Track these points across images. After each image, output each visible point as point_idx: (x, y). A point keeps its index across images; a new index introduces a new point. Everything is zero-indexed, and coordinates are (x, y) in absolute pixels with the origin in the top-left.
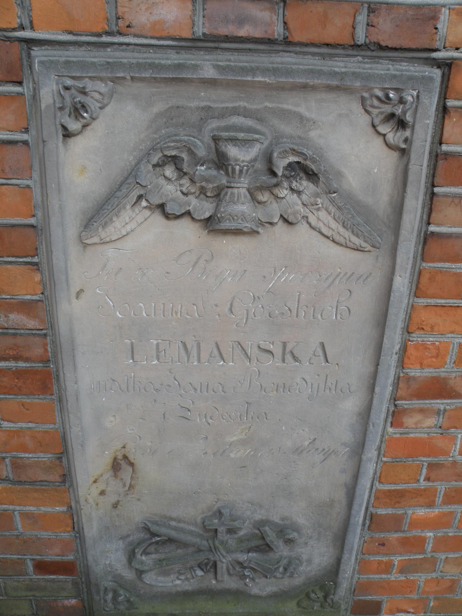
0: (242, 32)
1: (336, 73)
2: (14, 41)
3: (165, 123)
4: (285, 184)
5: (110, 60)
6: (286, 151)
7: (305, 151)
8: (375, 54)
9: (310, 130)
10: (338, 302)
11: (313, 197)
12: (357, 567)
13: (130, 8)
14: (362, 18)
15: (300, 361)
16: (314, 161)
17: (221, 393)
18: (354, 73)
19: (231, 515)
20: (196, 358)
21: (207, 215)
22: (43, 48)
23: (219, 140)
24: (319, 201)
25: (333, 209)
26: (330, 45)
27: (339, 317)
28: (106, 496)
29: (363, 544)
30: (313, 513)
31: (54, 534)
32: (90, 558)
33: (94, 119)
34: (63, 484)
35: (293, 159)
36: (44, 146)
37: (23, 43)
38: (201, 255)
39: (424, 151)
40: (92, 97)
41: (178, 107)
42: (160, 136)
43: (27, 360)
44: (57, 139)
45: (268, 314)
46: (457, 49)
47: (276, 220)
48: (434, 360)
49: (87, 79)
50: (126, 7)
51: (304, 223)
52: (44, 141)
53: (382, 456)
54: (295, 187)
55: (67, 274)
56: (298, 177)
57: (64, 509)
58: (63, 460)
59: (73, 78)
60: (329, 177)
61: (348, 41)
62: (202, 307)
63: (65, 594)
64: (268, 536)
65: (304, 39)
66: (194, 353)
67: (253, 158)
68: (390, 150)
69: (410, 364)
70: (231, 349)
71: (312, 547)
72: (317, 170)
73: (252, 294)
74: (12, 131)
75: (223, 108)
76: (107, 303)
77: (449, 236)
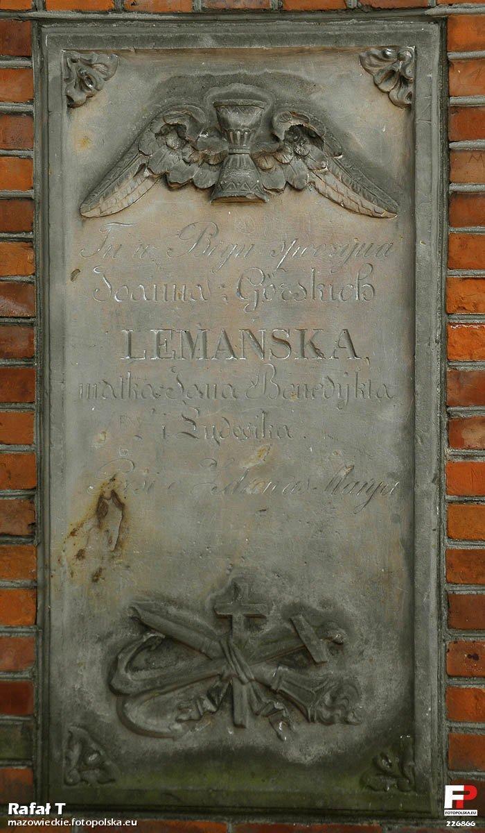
1: (330, 36)
4: (289, 149)
5: (116, 35)
6: (286, 114)
8: (368, 15)
11: (318, 160)
12: (443, 704)
15: (323, 354)
16: (316, 123)
18: (347, 35)
19: (251, 595)
20: (201, 352)
21: (210, 184)
26: (324, 11)
27: (362, 296)
29: (445, 655)
32: (54, 670)
33: (98, 90)
34: (30, 540)
37: (35, 22)
40: (97, 69)
41: (180, 77)
44: (62, 109)
47: (281, 187)
52: (49, 112)
55: (63, 249)
59: (80, 52)
63: (9, 753)
64: (303, 629)
65: (298, 8)
66: (200, 346)
67: (254, 123)
69: (457, 355)
70: (241, 340)
71: (371, 660)
75: (224, 76)
76: (104, 285)
77: (475, 195)
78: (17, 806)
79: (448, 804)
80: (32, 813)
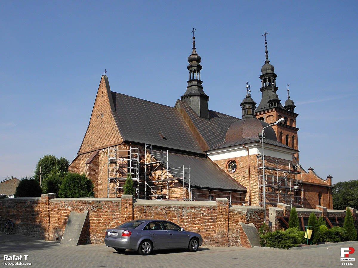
78: (7, 256)
79: (342, 256)
80: (14, 259)
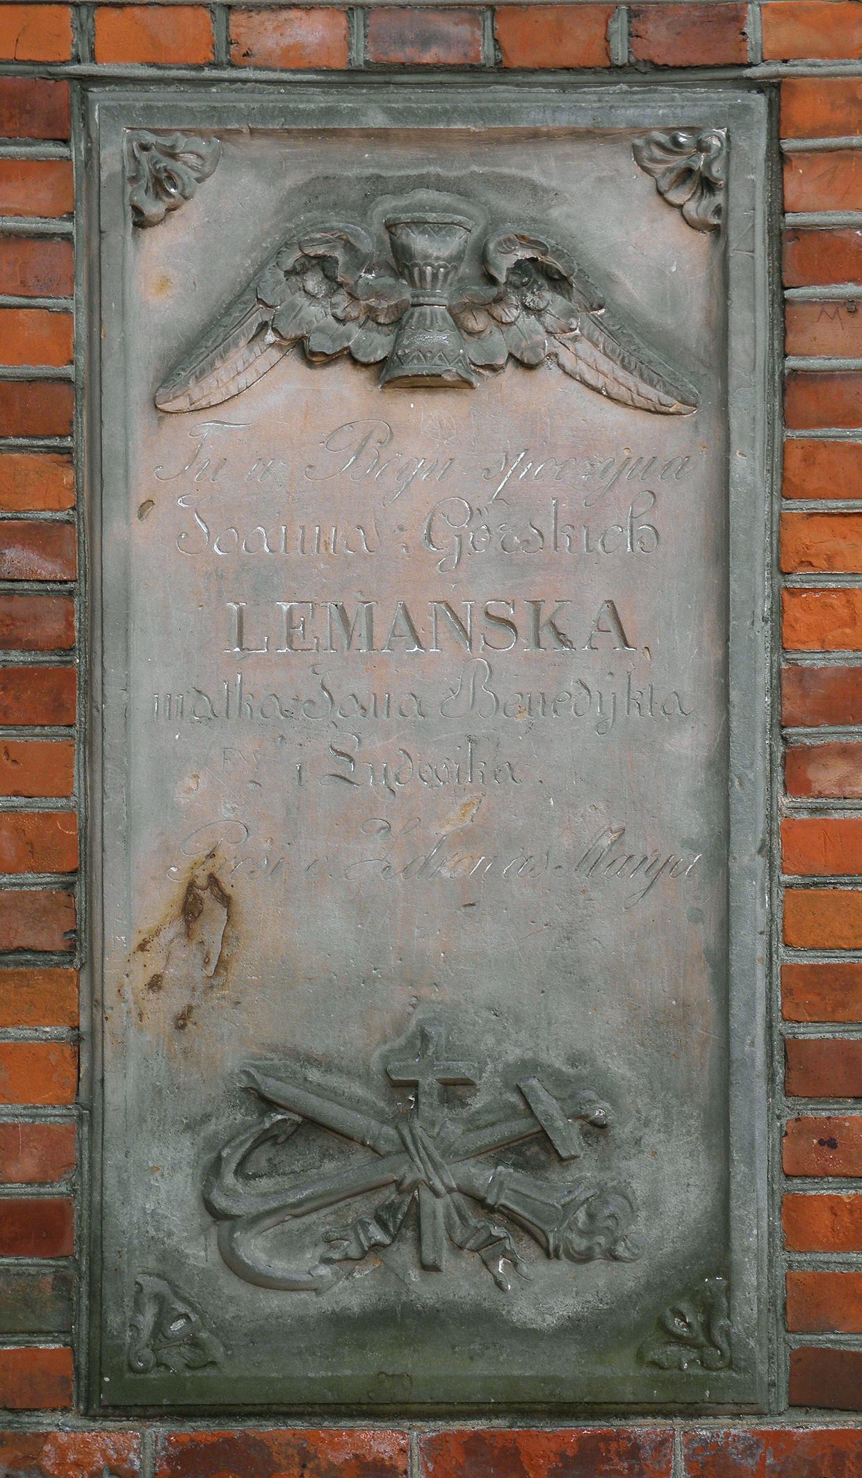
0: (428, 57)
2: (62, 79)
3: (306, 203)
4: (514, 299)
6: (509, 240)
7: (542, 239)
8: (648, 78)
9: (550, 207)
10: (632, 517)
11: (563, 317)
13: (249, 28)
14: (620, 26)
15: (570, 642)
16: (559, 255)
17: (415, 716)
21: (380, 355)
22: (107, 89)
23: (395, 225)
24: (574, 323)
25: (601, 338)
27: (637, 546)
28: (162, 993)
30: (643, 1045)
31: (29, 1112)
33: (186, 198)
34: (69, 958)
35: (523, 254)
36: (101, 238)
38: (372, 432)
39: (753, 226)
40: (185, 163)
42: (297, 225)
43: (28, 647)
45: (500, 543)
46: (785, 61)
47: (501, 361)
48: (848, 631)
49: (178, 134)
50: (242, 26)
51: (554, 367)
52: (101, 232)
53: (778, 872)
54: (531, 304)
56: (536, 286)
57: (63, 1030)
58: (77, 889)
59: (156, 132)
60: (588, 281)
61: (597, 59)
62: (375, 533)
65: (527, 63)
68: (695, 232)
72: (566, 272)
73: (466, 505)
74: (46, 218)
77: (828, 376)
